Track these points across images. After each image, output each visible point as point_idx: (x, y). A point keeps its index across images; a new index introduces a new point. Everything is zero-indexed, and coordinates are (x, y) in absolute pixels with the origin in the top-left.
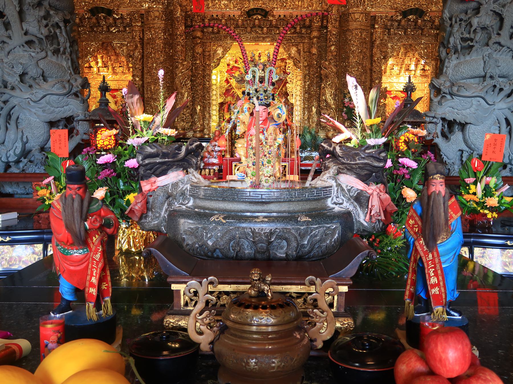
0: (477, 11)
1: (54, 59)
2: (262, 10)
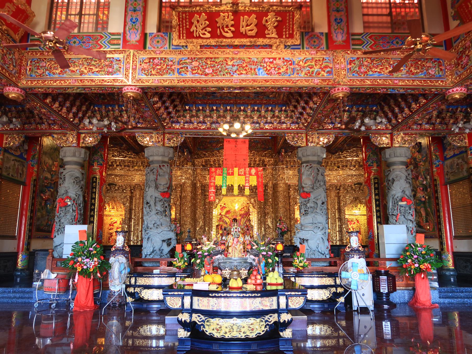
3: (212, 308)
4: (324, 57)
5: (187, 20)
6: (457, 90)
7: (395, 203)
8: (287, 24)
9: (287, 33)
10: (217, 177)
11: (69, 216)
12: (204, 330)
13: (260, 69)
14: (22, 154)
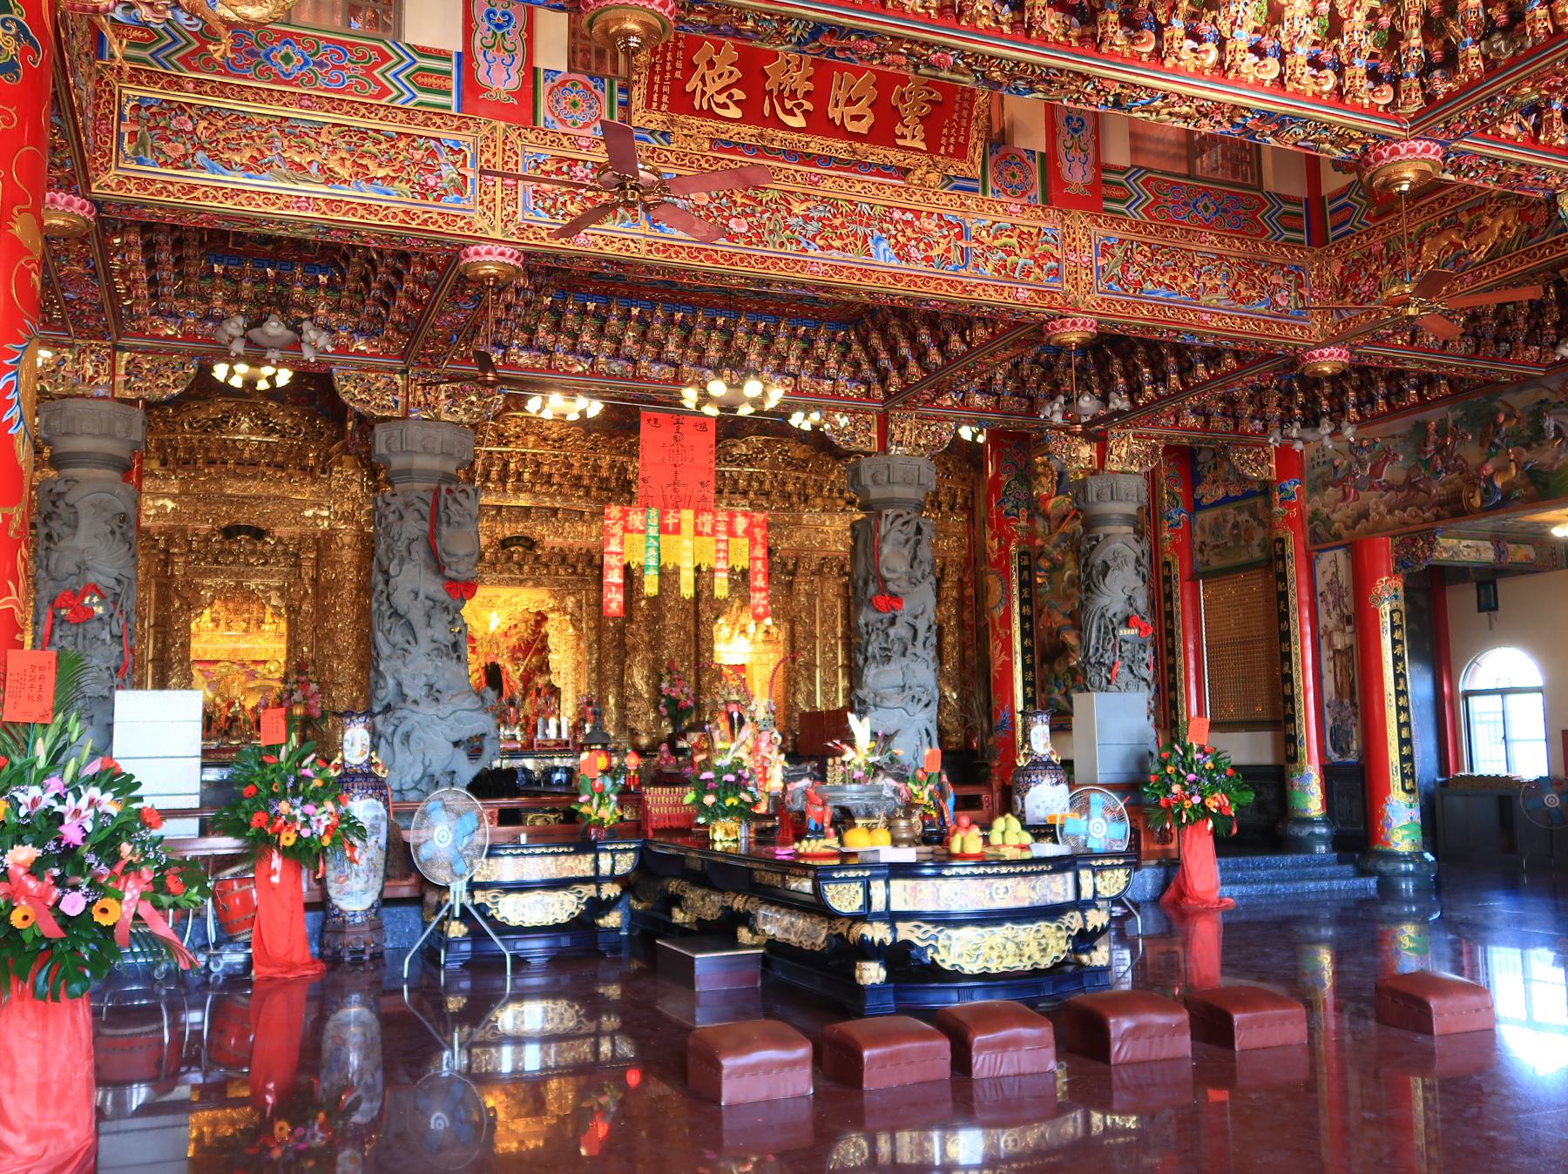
0: (893, 622)
2: (527, 539)
4: (1043, 225)
5: (680, 54)
6: (1331, 354)
7: (1109, 631)
9: (952, 140)
12: (938, 958)
13: (879, 239)
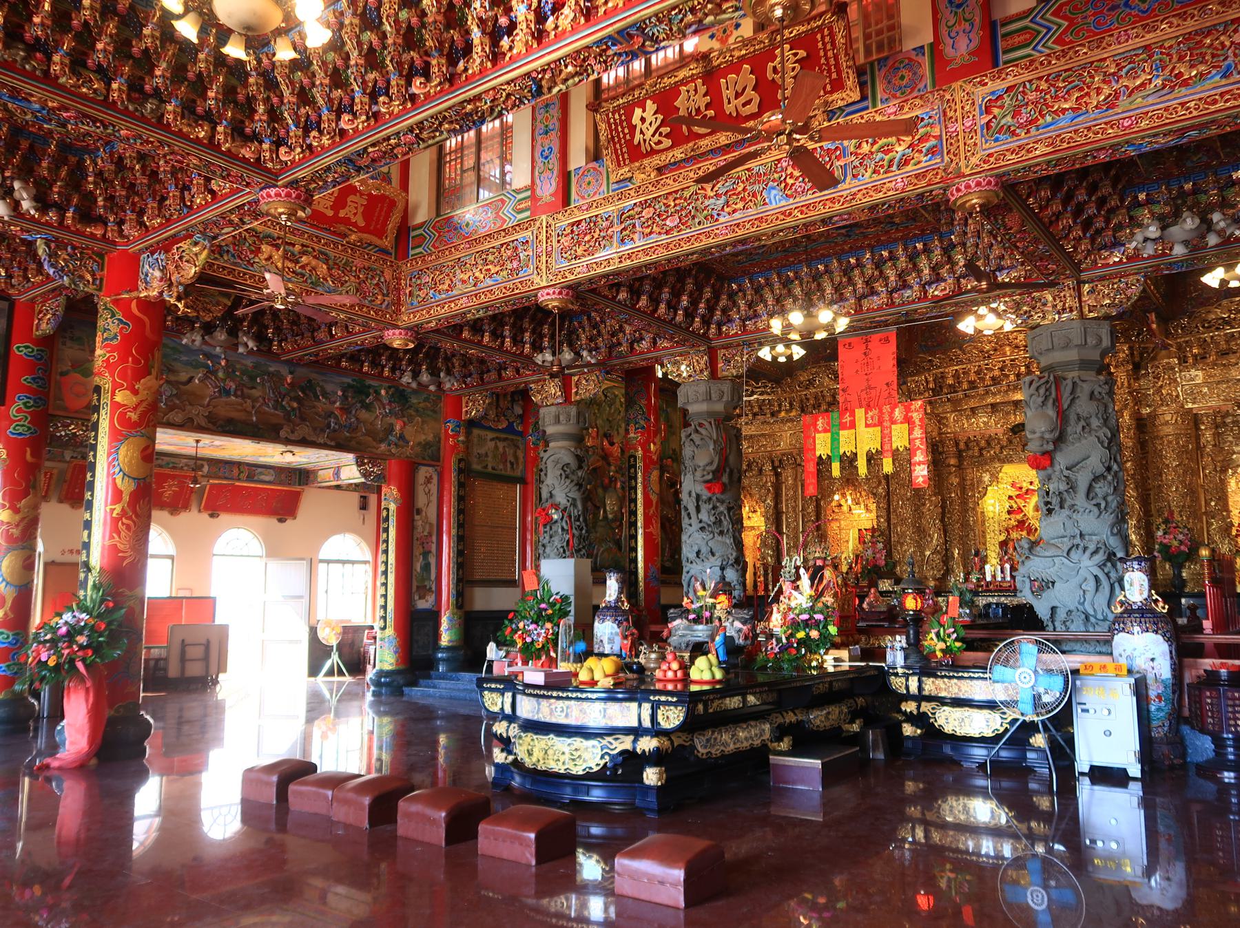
1: (720, 538)
3: (577, 719)
8: (823, 61)
10: (817, 435)
11: (557, 542)
14: (511, 424)
